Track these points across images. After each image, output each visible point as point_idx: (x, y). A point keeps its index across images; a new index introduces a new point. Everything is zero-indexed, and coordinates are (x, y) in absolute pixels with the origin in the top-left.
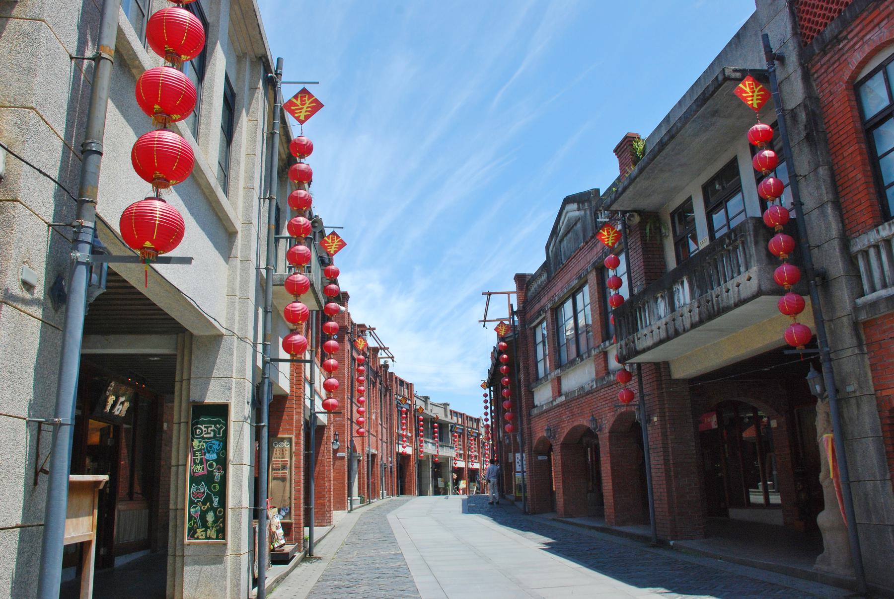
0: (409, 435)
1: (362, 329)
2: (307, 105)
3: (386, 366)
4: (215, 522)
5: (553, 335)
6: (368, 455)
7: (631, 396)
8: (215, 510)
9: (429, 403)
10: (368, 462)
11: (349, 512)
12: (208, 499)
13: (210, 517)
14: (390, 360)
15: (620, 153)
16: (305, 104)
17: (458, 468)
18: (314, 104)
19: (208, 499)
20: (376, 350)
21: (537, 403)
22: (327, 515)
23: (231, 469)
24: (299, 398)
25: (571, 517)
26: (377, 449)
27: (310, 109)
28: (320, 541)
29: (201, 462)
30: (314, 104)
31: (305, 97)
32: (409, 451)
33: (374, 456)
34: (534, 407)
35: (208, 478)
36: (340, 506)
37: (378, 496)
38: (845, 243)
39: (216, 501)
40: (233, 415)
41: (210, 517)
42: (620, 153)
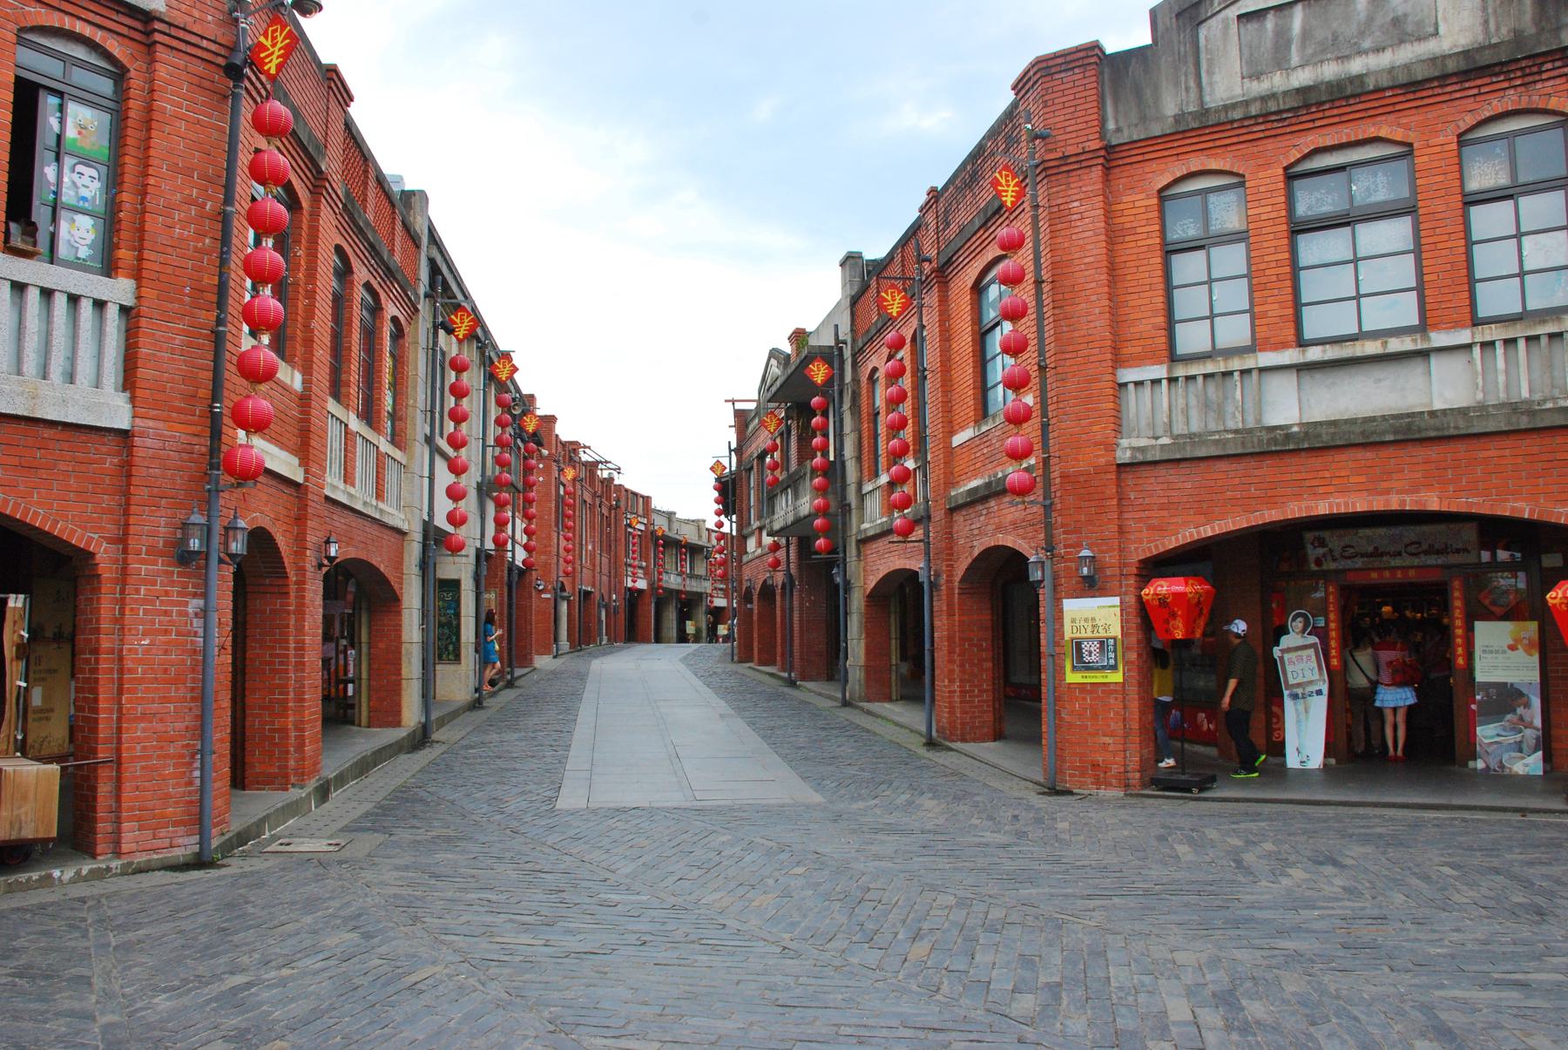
0: (644, 564)
1: (575, 447)
2: (279, 45)
3: (611, 479)
4: (454, 650)
5: (758, 485)
6: (580, 592)
7: (776, 564)
8: (453, 644)
9: (674, 520)
10: (580, 602)
11: (555, 657)
12: (449, 637)
13: (451, 648)
14: (615, 473)
15: (1023, 92)
16: (462, 323)
17: (716, 607)
18: (288, 41)
19: (449, 637)
20: (596, 464)
21: (748, 550)
22: (529, 657)
23: (463, 619)
24: (503, 557)
25: (765, 665)
26: (593, 586)
27: (282, 51)
28: (462, 556)
29: (445, 615)
30: (288, 41)
31: (275, 31)
32: (642, 584)
33: (587, 594)
34: (746, 553)
35: (449, 624)
36: (545, 650)
37: (595, 642)
38: (860, 485)
39: (454, 638)
40: (463, 587)
41: (451, 648)
42: (1023, 92)
